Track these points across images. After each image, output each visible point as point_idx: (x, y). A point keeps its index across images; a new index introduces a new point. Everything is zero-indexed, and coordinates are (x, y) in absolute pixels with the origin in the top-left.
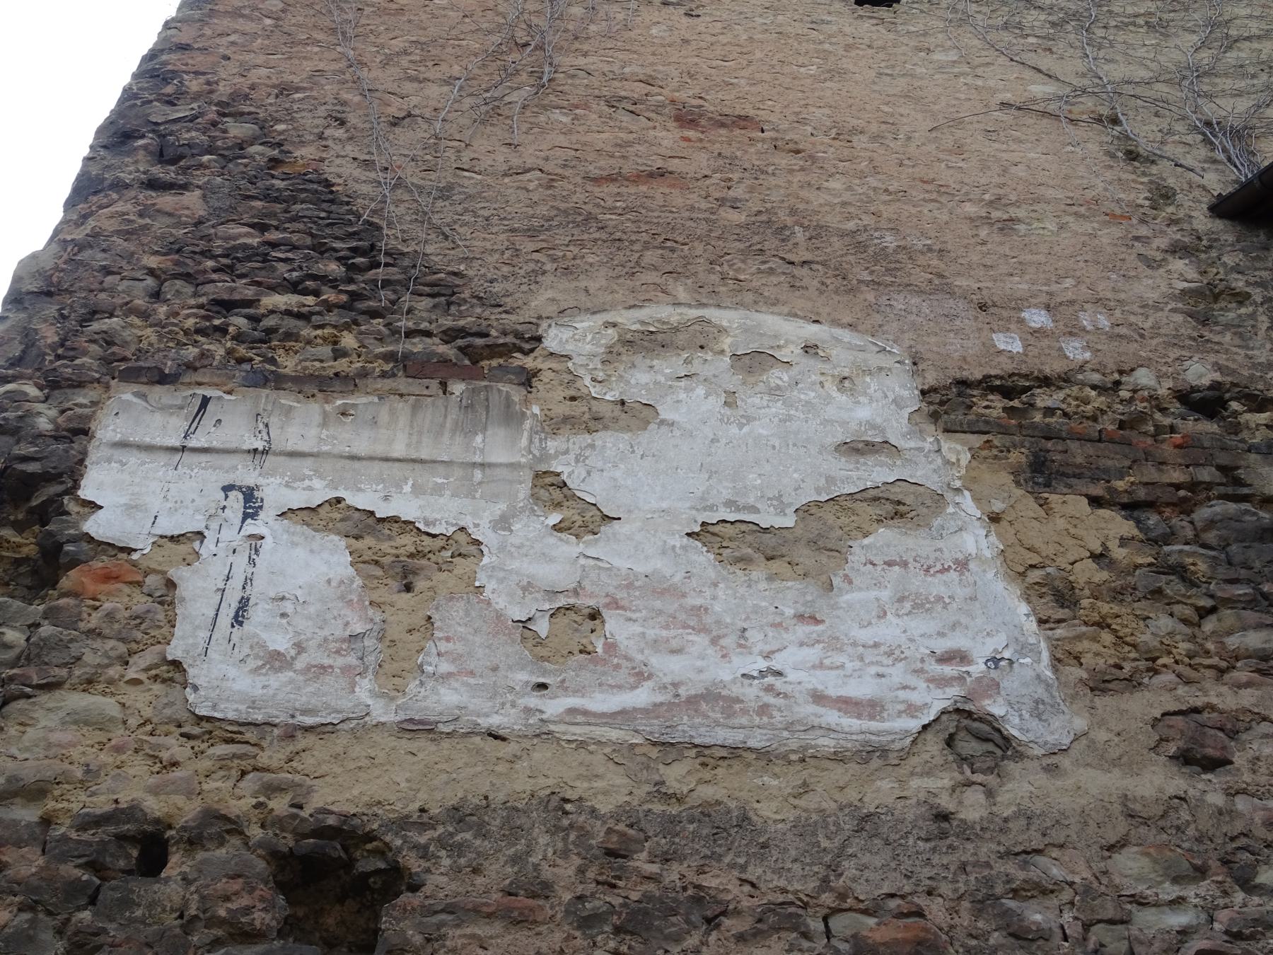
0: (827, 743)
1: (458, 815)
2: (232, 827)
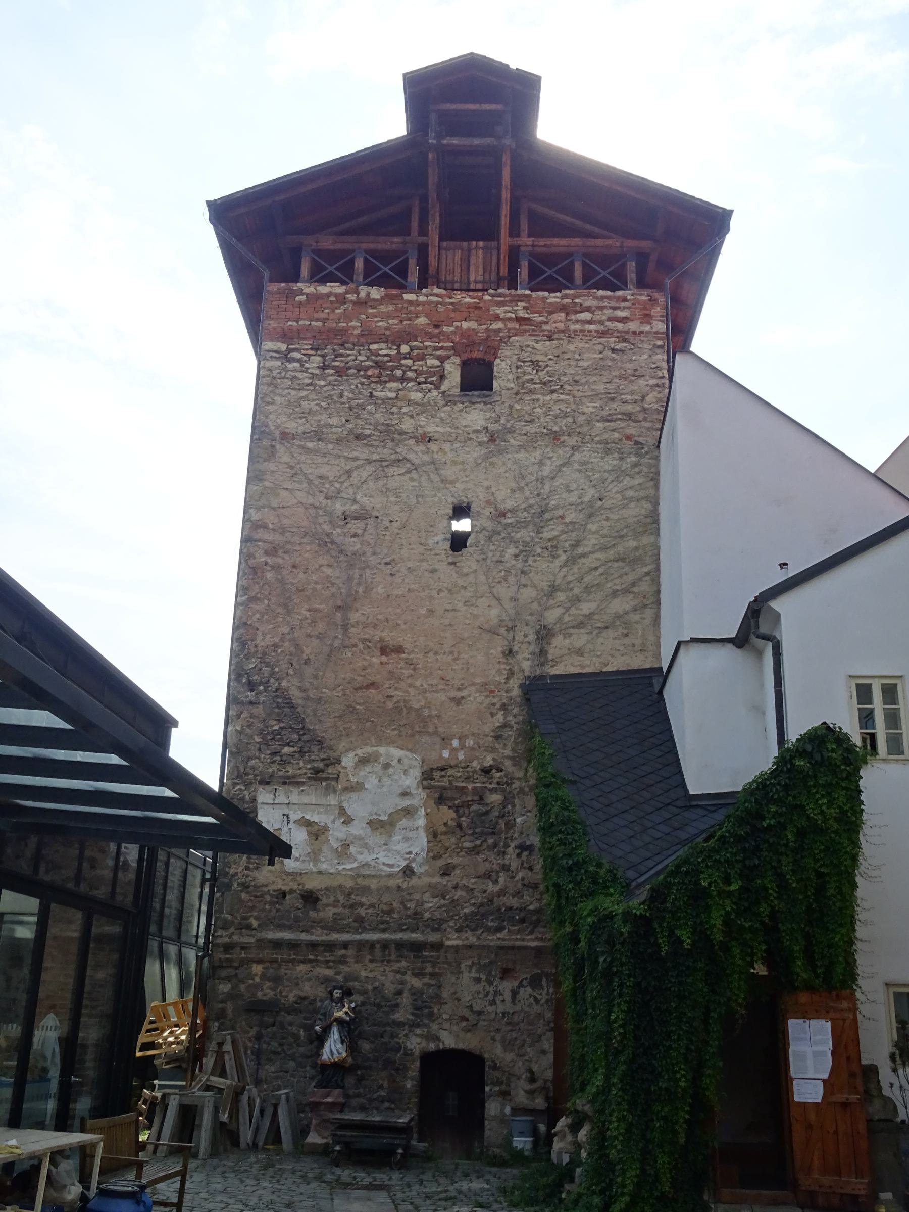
0: (384, 874)
1: (327, 889)
2: (295, 891)
